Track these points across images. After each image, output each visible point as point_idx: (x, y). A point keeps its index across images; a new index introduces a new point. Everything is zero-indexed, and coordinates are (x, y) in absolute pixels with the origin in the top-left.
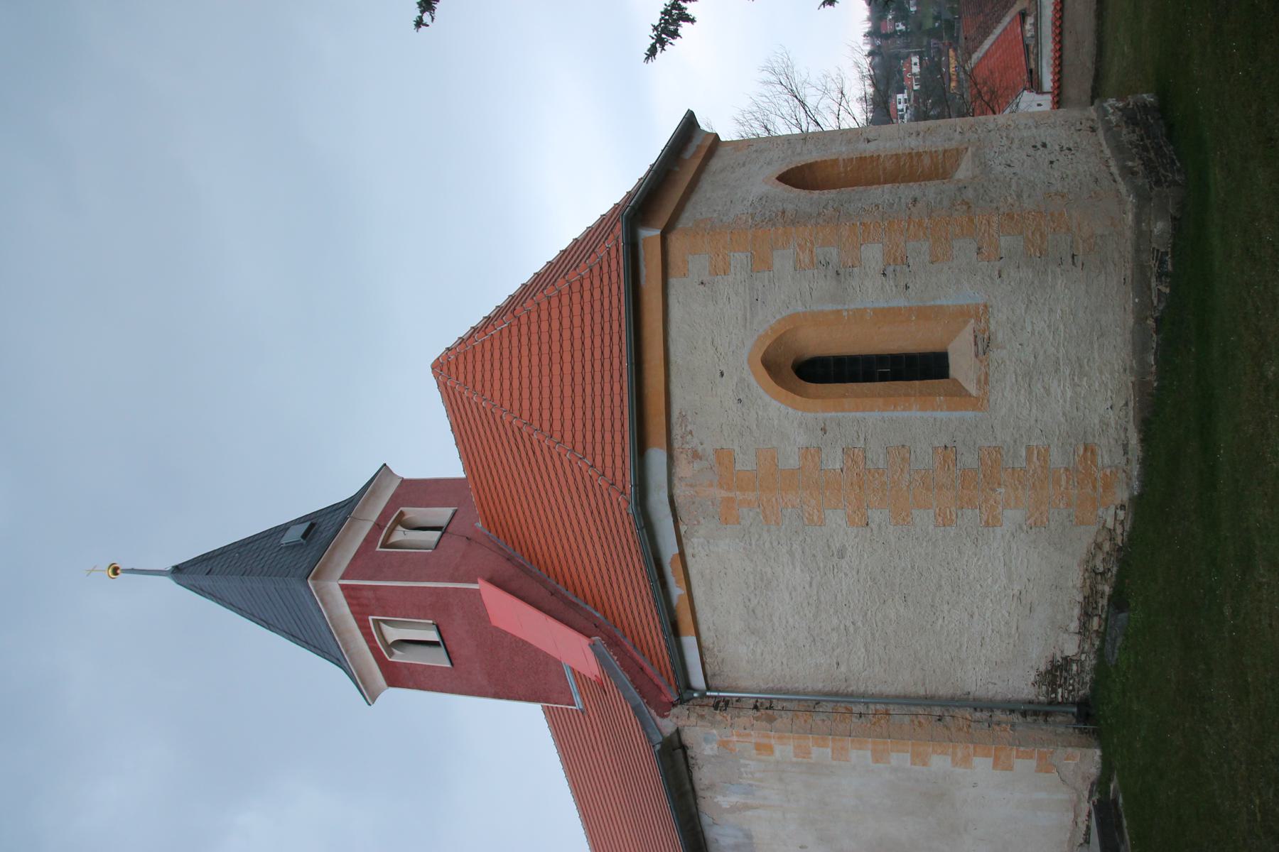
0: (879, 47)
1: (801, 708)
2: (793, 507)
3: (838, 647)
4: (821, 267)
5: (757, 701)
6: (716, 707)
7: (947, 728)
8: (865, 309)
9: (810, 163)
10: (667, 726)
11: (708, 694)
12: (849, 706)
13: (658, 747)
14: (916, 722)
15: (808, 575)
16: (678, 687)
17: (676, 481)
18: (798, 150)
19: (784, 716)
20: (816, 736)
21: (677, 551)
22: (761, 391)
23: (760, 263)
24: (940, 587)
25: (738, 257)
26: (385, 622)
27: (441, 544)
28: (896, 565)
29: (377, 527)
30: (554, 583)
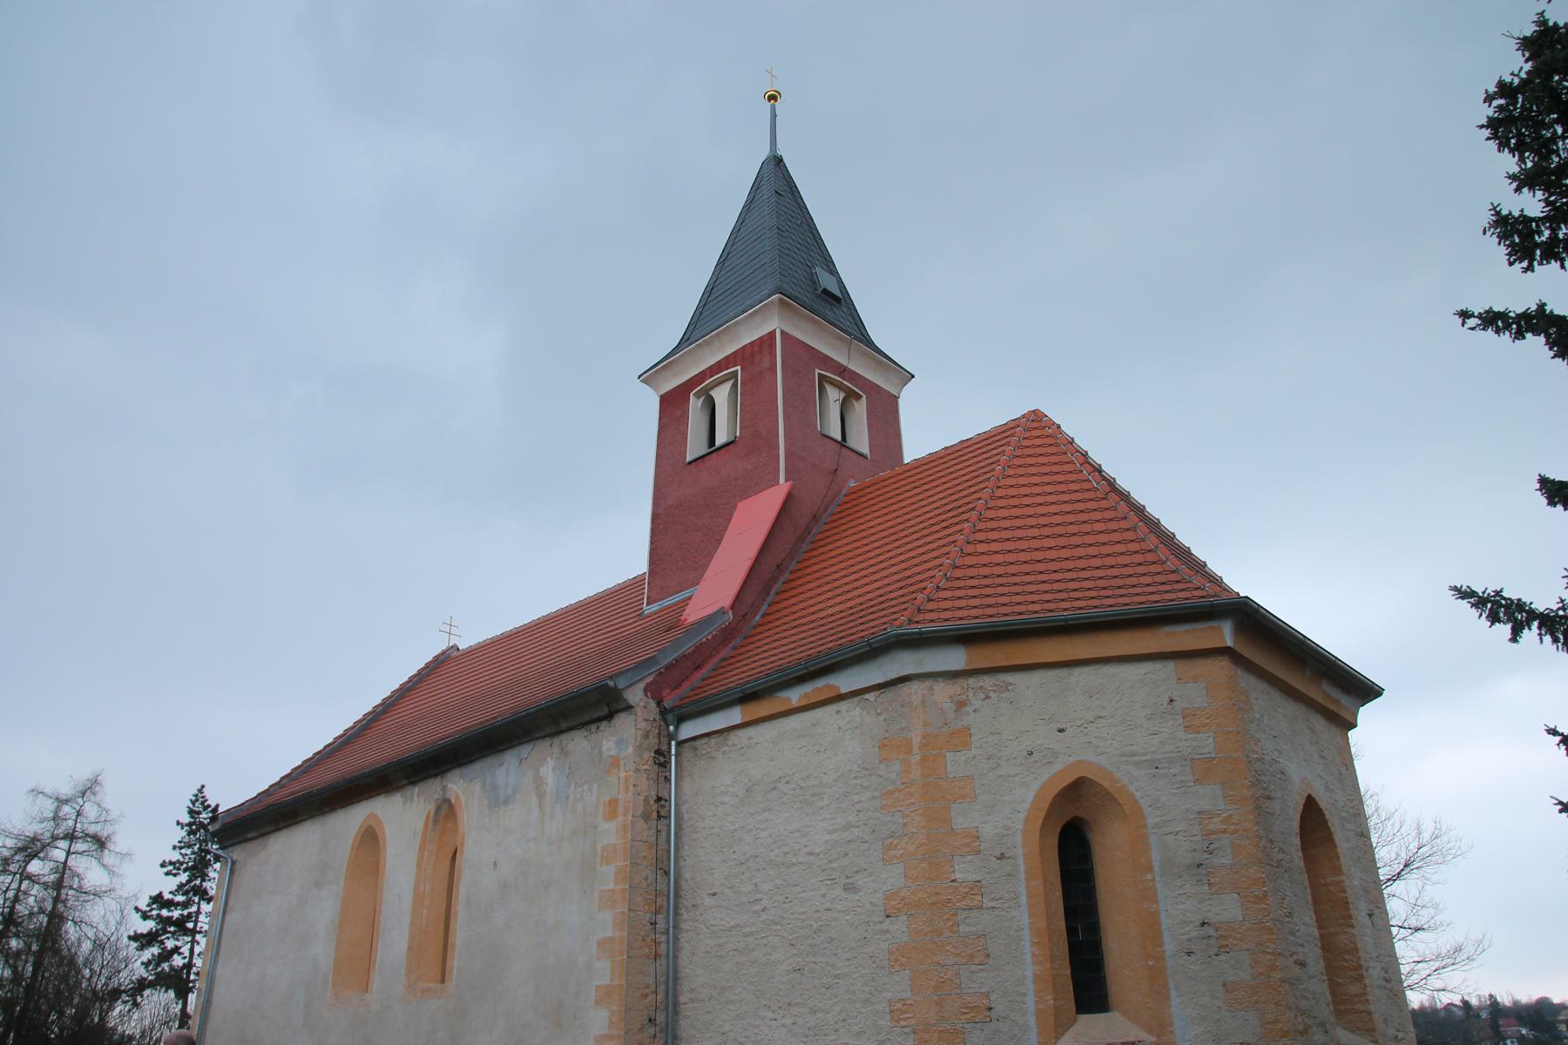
0: (1478, 1016)
1: (660, 852)
2: (905, 825)
3: (734, 893)
4: (1206, 844)
5: (666, 801)
6: (658, 752)
7: (641, 1029)
8: (1156, 902)
9: (1333, 839)
10: (635, 695)
11: (673, 743)
12: (664, 910)
13: (611, 683)
14: (646, 991)
15: (821, 849)
16: (679, 707)
17: (927, 683)
18: (1348, 826)
19: (651, 833)
20: (628, 869)
21: (844, 690)
22: (1045, 778)
23: (1203, 769)
24: (813, 1012)
25: (1208, 742)
26: (735, 385)
27: (827, 440)
28: (838, 956)
29: (842, 370)
30: (791, 568)
